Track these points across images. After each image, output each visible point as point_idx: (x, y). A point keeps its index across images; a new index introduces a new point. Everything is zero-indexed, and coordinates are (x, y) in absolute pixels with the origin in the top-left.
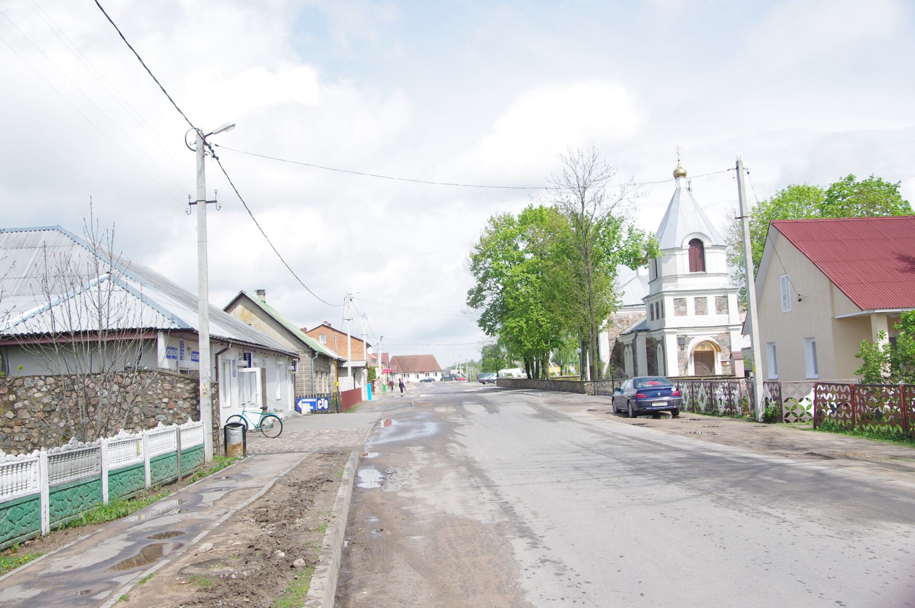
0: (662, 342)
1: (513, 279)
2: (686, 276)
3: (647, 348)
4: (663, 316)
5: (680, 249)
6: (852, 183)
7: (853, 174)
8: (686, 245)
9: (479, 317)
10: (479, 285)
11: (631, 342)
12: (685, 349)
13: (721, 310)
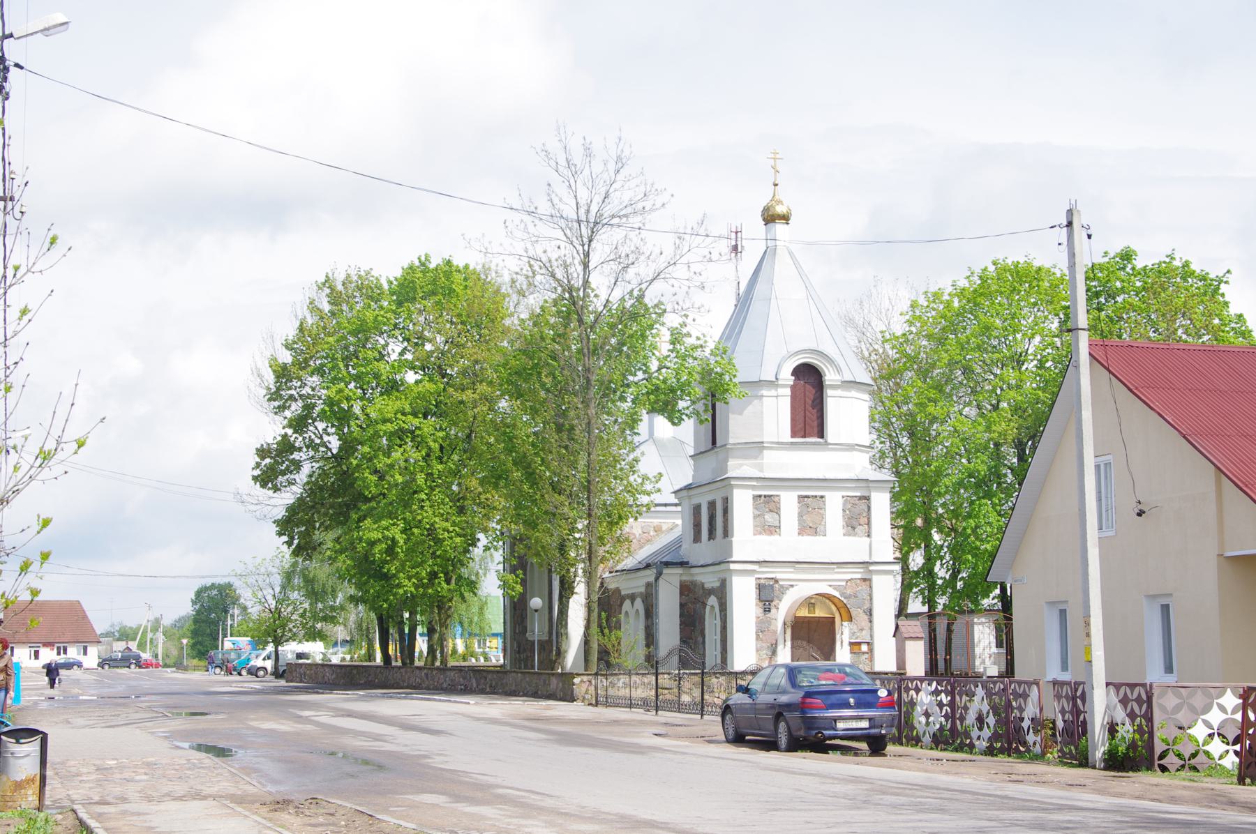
0: (722, 592)
1: (379, 427)
2: (781, 445)
3: (682, 606)
4: (727, 533)
5: (773, 384)
6: (1130, 266)
7: (1132, 247)
8: (787, 377)
9: (280, 513)
10: (285, 436)
11: (643, 590)
12: (773, 610)
13: (854, 528)
